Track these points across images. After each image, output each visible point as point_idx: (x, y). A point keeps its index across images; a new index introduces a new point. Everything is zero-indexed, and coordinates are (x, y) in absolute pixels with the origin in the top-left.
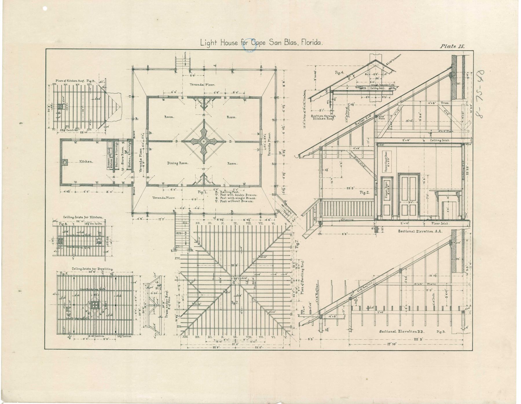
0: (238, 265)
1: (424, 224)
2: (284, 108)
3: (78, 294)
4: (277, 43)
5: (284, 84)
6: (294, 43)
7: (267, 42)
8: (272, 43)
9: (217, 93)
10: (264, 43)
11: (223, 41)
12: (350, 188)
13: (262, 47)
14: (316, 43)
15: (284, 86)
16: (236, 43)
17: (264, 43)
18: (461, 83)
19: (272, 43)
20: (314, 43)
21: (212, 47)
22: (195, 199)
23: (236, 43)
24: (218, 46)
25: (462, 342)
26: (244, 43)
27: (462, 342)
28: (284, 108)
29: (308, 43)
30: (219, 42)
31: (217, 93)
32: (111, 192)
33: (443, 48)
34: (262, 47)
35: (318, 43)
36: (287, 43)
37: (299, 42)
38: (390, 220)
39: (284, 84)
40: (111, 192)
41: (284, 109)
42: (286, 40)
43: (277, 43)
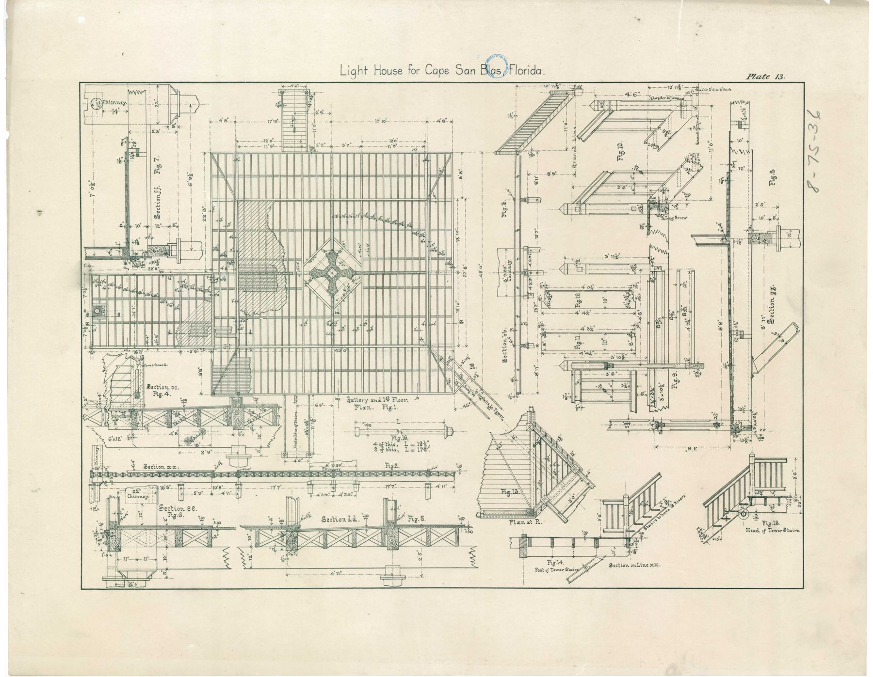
0: (346, 328)
1: (605, 301)
2: (190, 178)
3: (170, 337)
4: (468, 72)
7: (453, 70)
8: (459, 71)
10: (446, 71)
11: (378, 67)
12: (481, 272)
13: (444, 78)
14: (533, 72)
16: (400, 72)
17: (446, 71)
18: (556, 124)
19: (459, 71)
20: (530, 72)
21: (360, 78)
23: (400, 72)
24: (370, 76)
26: (414, 71)
28: (190, 178)
29: (521, 72)
30: (371, 70)
33: (751, 79)
34: (444, 78)
35: (536, 71)
38: (189, 474)
41: (190, 182)
43: (468, 72)
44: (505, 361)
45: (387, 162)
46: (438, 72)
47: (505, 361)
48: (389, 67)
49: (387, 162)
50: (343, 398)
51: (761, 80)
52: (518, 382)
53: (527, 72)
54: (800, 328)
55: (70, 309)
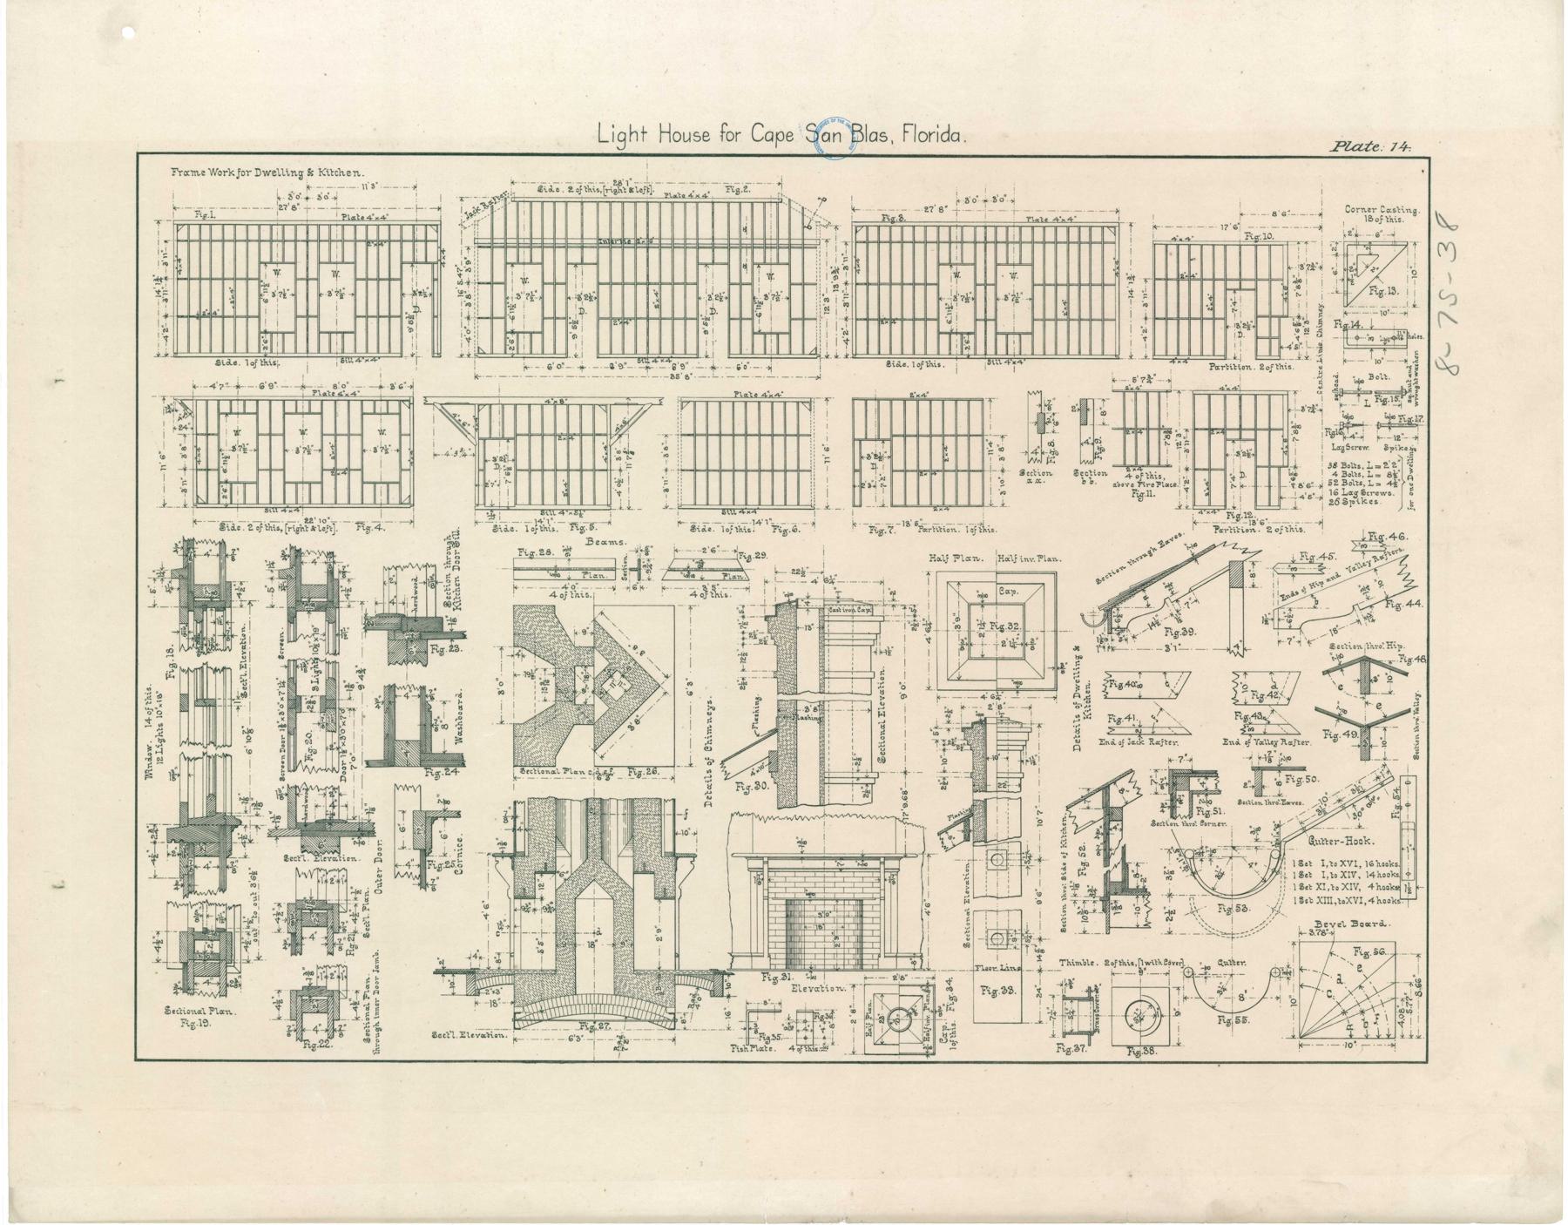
5: (690, 689)
6: (881, 136)
9: (271, 386)
14: (945, 137)
15: (1274, 214)
16: (705, 137)
17: (789, 136)
20: (940, 137)
22: (1039, 812)
24: (651, 144)
25: (832, 355)
26: (728, 135)
27: (832, 355)
29: (923, 137)
30: (653, 133)
31: (271, 386)
32: (904, 688)
34: (784, 147)
35: (951, 136)
36: (858, 136)
37: (895, 133)
39: (690, 689)
40: (904, 688)
42: (855, 128)
44: (1416, 757)
45: (714, 485)
46: (774, 137)
47: (1416, 757)
48: (686, 127)
49: (714, 485)
50: (1198, 971)
51: (1363, 153)
52: (924, 1058)
53: (934, 137)
54: (1074, 1057)
55: (122, 903)
